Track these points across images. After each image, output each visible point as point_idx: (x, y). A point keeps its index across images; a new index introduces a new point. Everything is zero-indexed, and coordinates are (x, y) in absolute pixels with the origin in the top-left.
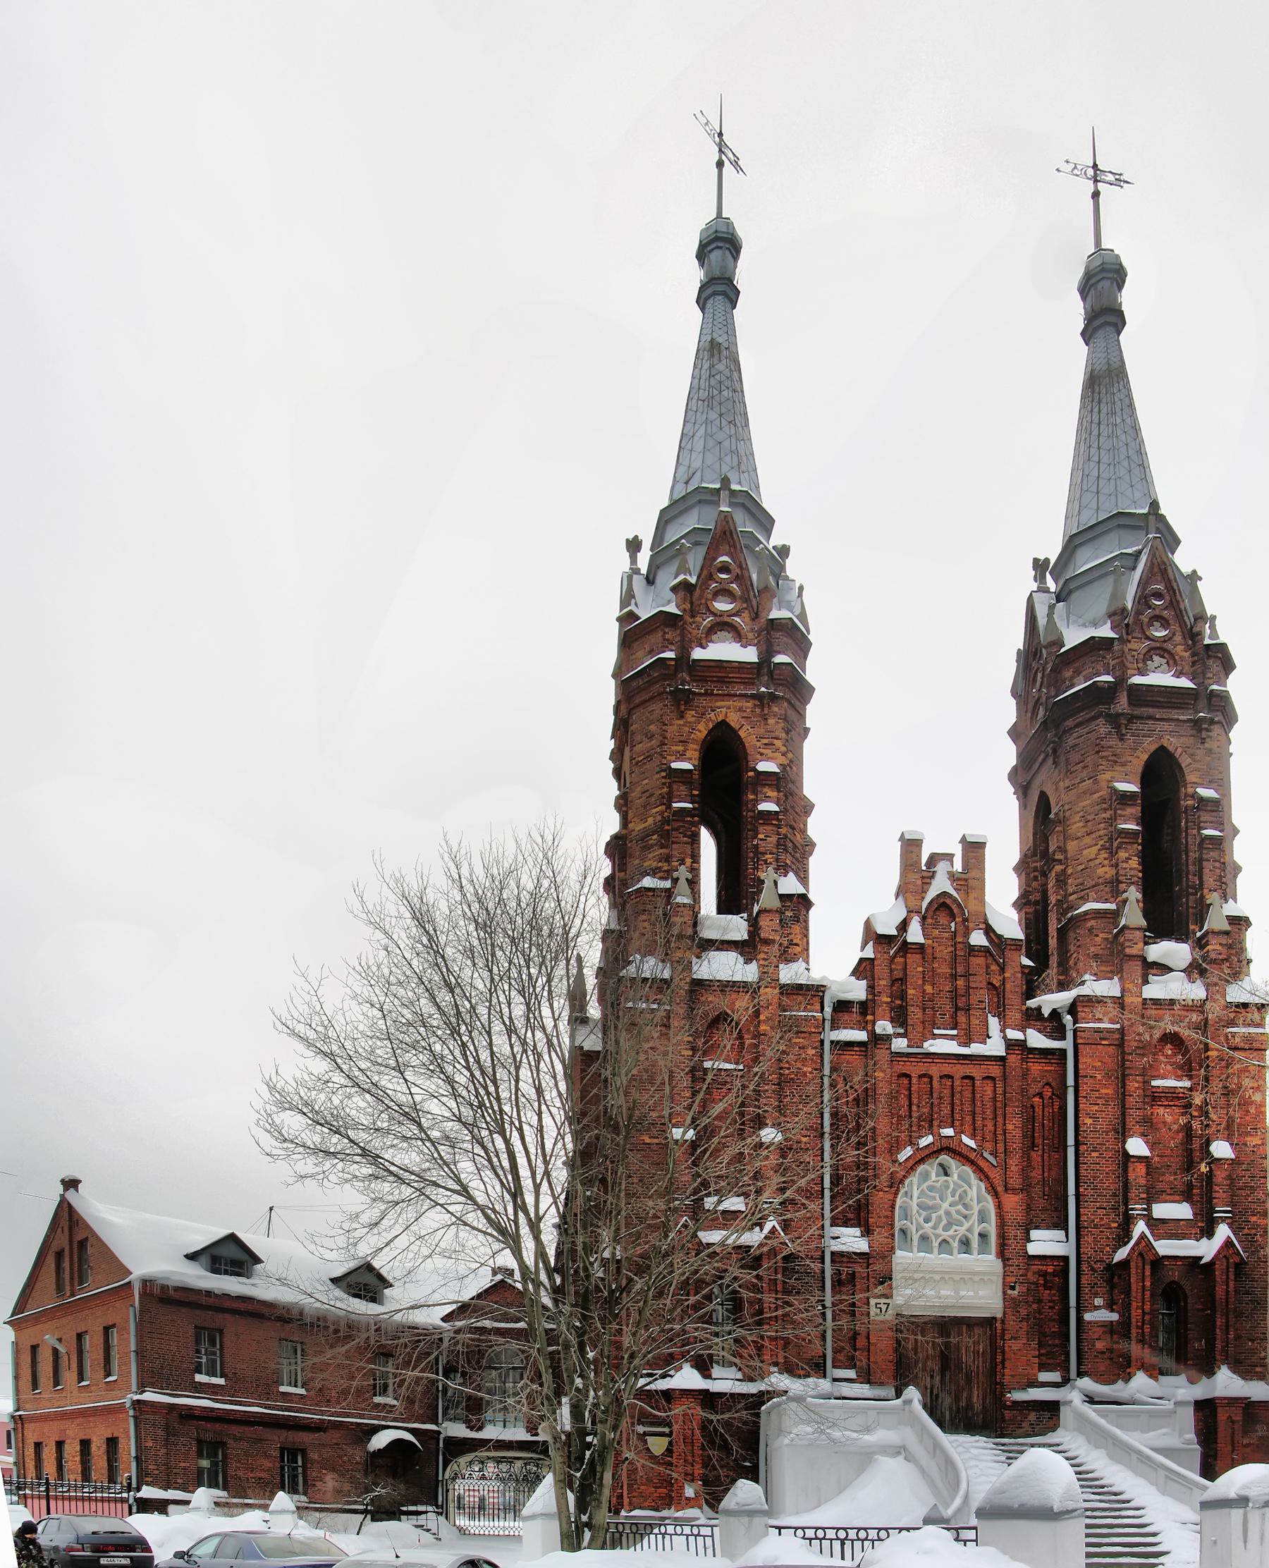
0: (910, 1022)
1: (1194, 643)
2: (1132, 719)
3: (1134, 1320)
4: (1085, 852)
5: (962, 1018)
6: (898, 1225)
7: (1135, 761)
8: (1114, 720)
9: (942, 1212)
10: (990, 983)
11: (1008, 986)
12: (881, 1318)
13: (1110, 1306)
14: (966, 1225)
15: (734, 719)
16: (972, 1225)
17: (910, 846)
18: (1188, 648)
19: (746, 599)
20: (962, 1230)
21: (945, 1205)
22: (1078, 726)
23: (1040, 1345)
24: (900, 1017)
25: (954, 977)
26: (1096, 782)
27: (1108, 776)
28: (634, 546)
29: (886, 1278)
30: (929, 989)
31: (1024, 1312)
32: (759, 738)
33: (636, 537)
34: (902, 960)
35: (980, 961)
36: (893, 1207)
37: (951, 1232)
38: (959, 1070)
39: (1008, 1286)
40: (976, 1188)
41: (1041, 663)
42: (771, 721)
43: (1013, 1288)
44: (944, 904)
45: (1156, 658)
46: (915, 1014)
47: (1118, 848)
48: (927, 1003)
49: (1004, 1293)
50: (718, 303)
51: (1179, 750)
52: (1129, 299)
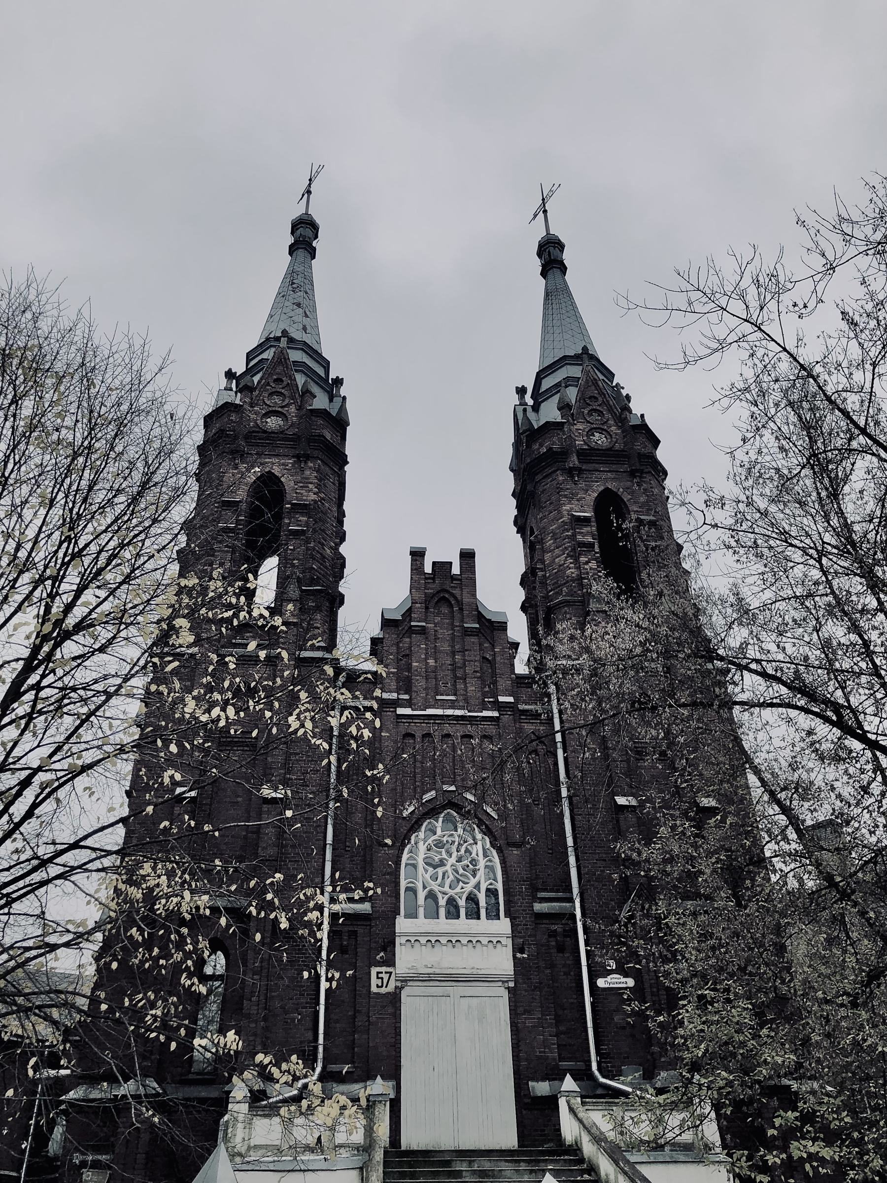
0: (414, 689)
1: (623, 425)
2: (580, 471)
3: (647, 985)
4: (557, 560)
5: (460, 686)
6: (403, 884)
7: (588, 498)
8: (570, 472)
9: (448, 868)
10: (484, 658)
11: (498, 659)
12: (383, 990)
13: (622, 970)
14: (473, 881)
15: (276, 470)
16: (479, 883)
17: (417, 555)
18: (619, 428)
19: (292, 397)
20: (469, 888)
21: (453, 860)
22: (544, 477)
23: (558, 1020)
24: (406, 685)
25: (453, 653)
26: (560, 512)
27: (567, 507)
28: (521, 391)
29: (388, 944)
30: (431, 662)
31: (535, 979)
32: (296, 483)
33: (523, 386)
34: (408, 640)
35: (474, 639)
36: (398, 863)
37: (458, 890)
38: (458, 731)
39: (518, 949)
40: (480, 845)
41: (526, 436)
42: (307, 473)
43: (522, 952)
44: (444, 598)
45: (596, 434)
46: (419, 683)
47: (580, 554)
48: (430, 674)
49: (514, 956)
50: (301, 253)
51: (621, 490)
52: (568, 257)
